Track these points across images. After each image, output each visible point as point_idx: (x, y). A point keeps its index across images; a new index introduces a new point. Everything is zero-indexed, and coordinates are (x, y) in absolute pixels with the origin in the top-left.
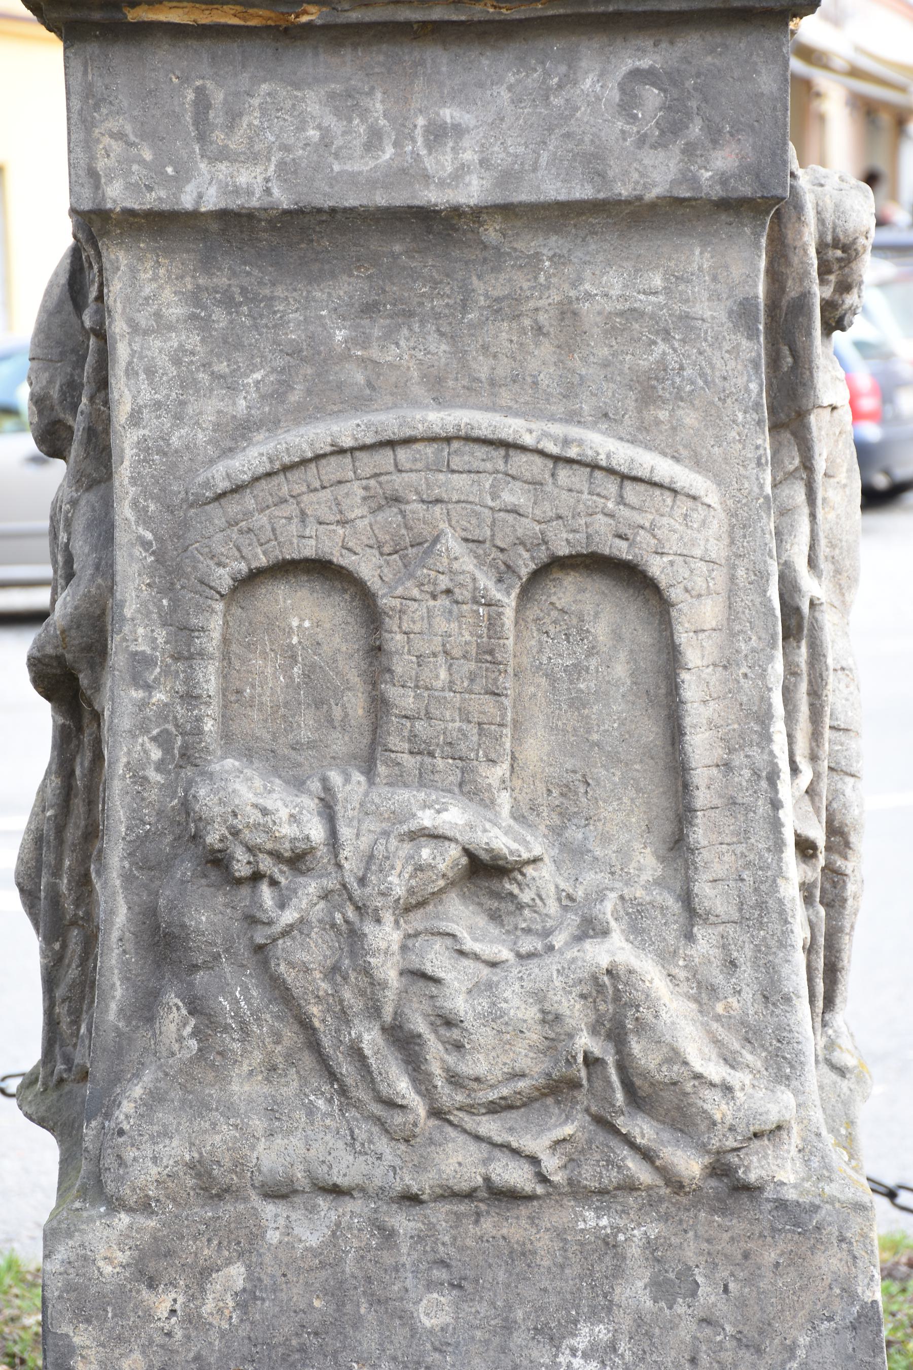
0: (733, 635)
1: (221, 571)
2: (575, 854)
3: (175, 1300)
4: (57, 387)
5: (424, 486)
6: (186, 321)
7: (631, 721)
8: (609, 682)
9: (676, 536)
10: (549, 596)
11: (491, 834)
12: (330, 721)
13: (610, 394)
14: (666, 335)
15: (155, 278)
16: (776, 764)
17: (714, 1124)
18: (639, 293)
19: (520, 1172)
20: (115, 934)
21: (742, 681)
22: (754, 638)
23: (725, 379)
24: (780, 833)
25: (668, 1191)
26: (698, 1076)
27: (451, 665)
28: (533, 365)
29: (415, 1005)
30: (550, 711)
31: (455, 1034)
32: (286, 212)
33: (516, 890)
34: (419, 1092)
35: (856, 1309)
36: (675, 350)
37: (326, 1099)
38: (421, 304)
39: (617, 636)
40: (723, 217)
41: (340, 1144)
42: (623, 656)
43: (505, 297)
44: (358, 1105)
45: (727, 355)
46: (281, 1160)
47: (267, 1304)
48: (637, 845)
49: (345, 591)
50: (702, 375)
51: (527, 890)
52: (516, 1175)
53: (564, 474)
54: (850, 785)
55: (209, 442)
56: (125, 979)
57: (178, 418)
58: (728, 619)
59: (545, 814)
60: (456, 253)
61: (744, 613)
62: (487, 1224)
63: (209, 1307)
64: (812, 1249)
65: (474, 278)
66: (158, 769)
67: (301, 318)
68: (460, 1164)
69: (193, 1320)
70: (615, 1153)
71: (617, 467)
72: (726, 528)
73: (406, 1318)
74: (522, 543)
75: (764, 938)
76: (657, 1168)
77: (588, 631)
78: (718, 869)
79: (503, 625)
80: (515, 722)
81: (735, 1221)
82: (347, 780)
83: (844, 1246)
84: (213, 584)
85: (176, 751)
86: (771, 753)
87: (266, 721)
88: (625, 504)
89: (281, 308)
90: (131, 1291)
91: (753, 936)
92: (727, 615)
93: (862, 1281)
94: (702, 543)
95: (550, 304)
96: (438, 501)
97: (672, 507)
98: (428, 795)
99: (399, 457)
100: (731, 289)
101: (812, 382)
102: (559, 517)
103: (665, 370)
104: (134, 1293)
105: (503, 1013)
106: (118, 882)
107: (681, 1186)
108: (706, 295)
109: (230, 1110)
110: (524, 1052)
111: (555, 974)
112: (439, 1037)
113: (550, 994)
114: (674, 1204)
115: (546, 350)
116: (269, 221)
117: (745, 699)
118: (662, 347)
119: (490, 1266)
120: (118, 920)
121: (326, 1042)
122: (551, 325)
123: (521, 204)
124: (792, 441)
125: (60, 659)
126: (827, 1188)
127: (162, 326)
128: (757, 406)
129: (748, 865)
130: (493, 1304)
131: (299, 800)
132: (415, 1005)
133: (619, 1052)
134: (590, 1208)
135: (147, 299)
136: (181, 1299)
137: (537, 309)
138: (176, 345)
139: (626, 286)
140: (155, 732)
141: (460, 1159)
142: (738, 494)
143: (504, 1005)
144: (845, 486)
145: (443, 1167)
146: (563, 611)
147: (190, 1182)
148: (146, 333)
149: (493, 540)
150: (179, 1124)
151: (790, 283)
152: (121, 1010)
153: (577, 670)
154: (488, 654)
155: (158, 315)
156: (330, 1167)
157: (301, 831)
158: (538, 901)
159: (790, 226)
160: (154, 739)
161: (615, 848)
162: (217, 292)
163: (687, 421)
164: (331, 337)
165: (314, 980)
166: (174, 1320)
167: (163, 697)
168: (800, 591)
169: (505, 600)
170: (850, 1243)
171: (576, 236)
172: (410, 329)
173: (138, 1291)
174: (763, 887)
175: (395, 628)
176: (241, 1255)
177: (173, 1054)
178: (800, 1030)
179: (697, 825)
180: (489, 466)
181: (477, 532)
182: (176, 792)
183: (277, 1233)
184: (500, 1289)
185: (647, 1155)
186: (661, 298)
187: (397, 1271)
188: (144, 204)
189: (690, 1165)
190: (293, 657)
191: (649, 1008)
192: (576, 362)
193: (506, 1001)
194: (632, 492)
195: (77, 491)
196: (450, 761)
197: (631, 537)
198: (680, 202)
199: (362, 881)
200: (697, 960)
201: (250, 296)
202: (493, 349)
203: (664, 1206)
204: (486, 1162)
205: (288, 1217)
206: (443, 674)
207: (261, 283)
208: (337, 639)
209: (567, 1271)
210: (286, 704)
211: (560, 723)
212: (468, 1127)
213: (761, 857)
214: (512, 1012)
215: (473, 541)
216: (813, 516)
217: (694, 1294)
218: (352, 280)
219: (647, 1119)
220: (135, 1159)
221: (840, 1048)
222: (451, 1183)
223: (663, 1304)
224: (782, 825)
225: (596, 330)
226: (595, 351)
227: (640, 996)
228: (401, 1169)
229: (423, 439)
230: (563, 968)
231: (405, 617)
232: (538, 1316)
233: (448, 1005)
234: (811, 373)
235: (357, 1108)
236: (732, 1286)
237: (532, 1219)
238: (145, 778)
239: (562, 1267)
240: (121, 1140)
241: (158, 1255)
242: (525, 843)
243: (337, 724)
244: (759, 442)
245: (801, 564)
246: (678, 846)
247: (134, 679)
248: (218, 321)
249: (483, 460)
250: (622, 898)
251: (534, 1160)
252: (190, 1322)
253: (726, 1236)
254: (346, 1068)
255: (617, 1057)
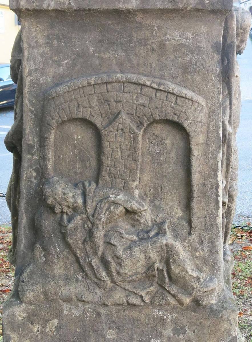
0: (207, 145)
1: (54, 121)
2: (156, 208)
3: (38, 328)
4: (17, 64)
5: (116, 97)
6: (45, 44)
7: (176, 170)
8: (170, 158)
9: (192, 115)
10: (153, 131)
11: (132, 203)
12: (86, 166)
13: (174, 70)
14: (192, 52)
15: (36, 31)
16: (219, 184)
17: (194, 288)
18: (184, 39)
19: (137, 300)
20: (23, 225)
21: (210, 159)
22: (214, 146)
23: (209, 66)
24: (218, 204)
25: (179, 306)
26: (190, 275)
27: (122, 151)
28: (150, 60)
29: (108, 252)
30: (151, 166)
31: (119, 261)
32: (76, 10)
33: (139, 219)
34: (108, 276)
35: (230, 338)
36: (194, 57)
37: (81, 277)
38: (117, 40)
39: (173, 144)
40: (211, 16)
41: (85, 289)
42: (174, 150)
43: (143, 39)
44: (90, 279)
45: (210, 59)
46: (68, 293)
47: (64, 330)
48: (176, 206)
49: (91, 128)
50: (203, 65)
51: (142, 218)
52: (136, 300)
53: (158, 94)
54: (235, 184)
55: (51, 81)
56: (26, 238)
57: (42, 74)
58: (207, 140)
59: (149, 196)
60: (128, 24)
61: (211, 139)
62: (127, 312)
63: (48, 330)
64: (220, 322)
65: (133, 33)
66: (35, 179)
67: (80, 44)
68: (120, 297)
69: (44, 333)
70: (164, 295)
71: (175, 93)
72: (207, 112)
73: (104, 337)
74: (145, 115)
75: (212, 234)
76: (177, 300)
77: (164, 142)
78: (199, 215)
79: (138, 140)
80: (141, 169)
81: (198, 314)
82: (90, 185)
83: (229, 321)
84: (51, 125)
85: (40, 174)
86: (217, 181)
87: (67, 166)
88: (177, 104)
89: (74, 41)
90: (26, 324)
91: (208, 234)
92: (206, 139)
93: (233, 330)
94: (200, 117)
95: (156, 41)
96: (120, 102)
97: (192, 106)
98: (114, 190)
99: (108, 87)
100: (213, 39)
101: (233, 68)
102: (157, 108)
103: (191, 63)
104: (27, 325)
105: (134, 256)
106: (23, 211)
107: (183, 305)
108: (205, 40)
109: (54, 278)
110: (139, 266)
111: (149, 245)
112: (114, 261)
113: (148, 251)
114: (181, 309)
115: (155, 56)
116: (70, 13)
117: (210, 164)
118: (190, 56)
119: (127, 323)
120: (23, 221)
121: (81, 261)
122: (156, 48)
123: (148, 9)
124: (226, 86)
125: (12, 143)
126: (225, 305)
127: (38, 45)
128: (219, 75)
129: (208, 213)
130: (127, 333)
131: (75, 190)
132: (108, 252)
133: (167, 267)
134: (157, 309)
135: (33, 37)
136: (40, 327)
137: (152, 43)
138: (42, 51)
139: (180, 37)
140: (34, 168)
141: (120, 295)
142: (212, 102)
143: (134, 253)
144: (238, 99)
145: (115, 297)
146: (157, 136)
147: (42, 296)
148: (33, 47)
149: (136, 114)
150: (39, 281)
151: (228, 39)
152: (25, 247)
153: (160, 154)
154: (134, 149)
155: (37, 42)
156: (82, 295)
157: (75, 200)
158: (145, 222)
159: (229, 21)
160: (34, 170)
161: (169, 207)
162: (55, 35)
163: (197, 79)
164: (89, 50)
165: (78, 244)
166: (38, 332)
167: (36, 158)
168: (226, 130)
169: (139, 132)
170: (230, 321)
171: (166, 20)
172: (113, 48)
173: (28, 325)
174: (212, 220)
175: (106, 140)
176: (57, 317)
177: (38, 261)
178: (220, 260)
179: (193, 202)
180: (136, 91)
181: (131, 111)
182: (40, 186)
183: (67, 312)
184: (130, 330)
185: (174, 296)
186: (191, 41)
187: (101, 323)
188: (32, 7)
189: (187, 300)
190: (75, 147)
191: (177, 256)
192: (163, 59)
193: (135, 252)
194: (179, 101)
195: (19, 94)
196: (121, 180)
197: (178, 115)
198: (198, 10)
199: (93, 216)
200: (191, 241)
201: (65, 37)
202: (138, 55)
203: (178, 309)
204: (127, 296)
205: (70, 307)
206: (119, 154)
207: (68, 33)
208: (88, 142)
209: (149, 325)
210: (73, 161)
211: (154, 169)
212: (122, 286)
213: (212, 211)
214: (136, 256)
215: (130, 114)
216: (231, 108)
217: (185, 333)
218: (95, 32)
219: (175, 286)
220: (27, 290)
221: (227, 254)
222: (117, 301)
223: (176, 335)
224: (219, 202)
225: (170, 50)
226: (170, 56)
227: (174, 252)
228: (102, 297)
229: (116, 82)
230: (152, 244)
231: (108, 137)
232: (140, 337)
233: (117, 253)
234: (233, 66)
235: (90, 280)
236: (196, 331)
237: (140, 312)
238: (31, 181)
239: (148, 324)
240: (23, 284)
241: (33, 315)
242: (142, 206)
243: (88, 167)
244: (219, 86)
245: (227, 122)
246: (188, 207)
247: (28, 151)
248: (55, 44)
249: (134, 89)
250: (170, 222)
251: (142, 297)
252: (43, 334)
253: (195, 318)
254: (87, 269)
255: (167, 268)
